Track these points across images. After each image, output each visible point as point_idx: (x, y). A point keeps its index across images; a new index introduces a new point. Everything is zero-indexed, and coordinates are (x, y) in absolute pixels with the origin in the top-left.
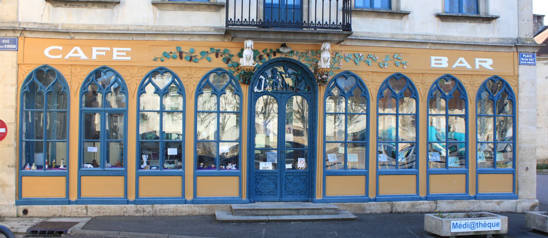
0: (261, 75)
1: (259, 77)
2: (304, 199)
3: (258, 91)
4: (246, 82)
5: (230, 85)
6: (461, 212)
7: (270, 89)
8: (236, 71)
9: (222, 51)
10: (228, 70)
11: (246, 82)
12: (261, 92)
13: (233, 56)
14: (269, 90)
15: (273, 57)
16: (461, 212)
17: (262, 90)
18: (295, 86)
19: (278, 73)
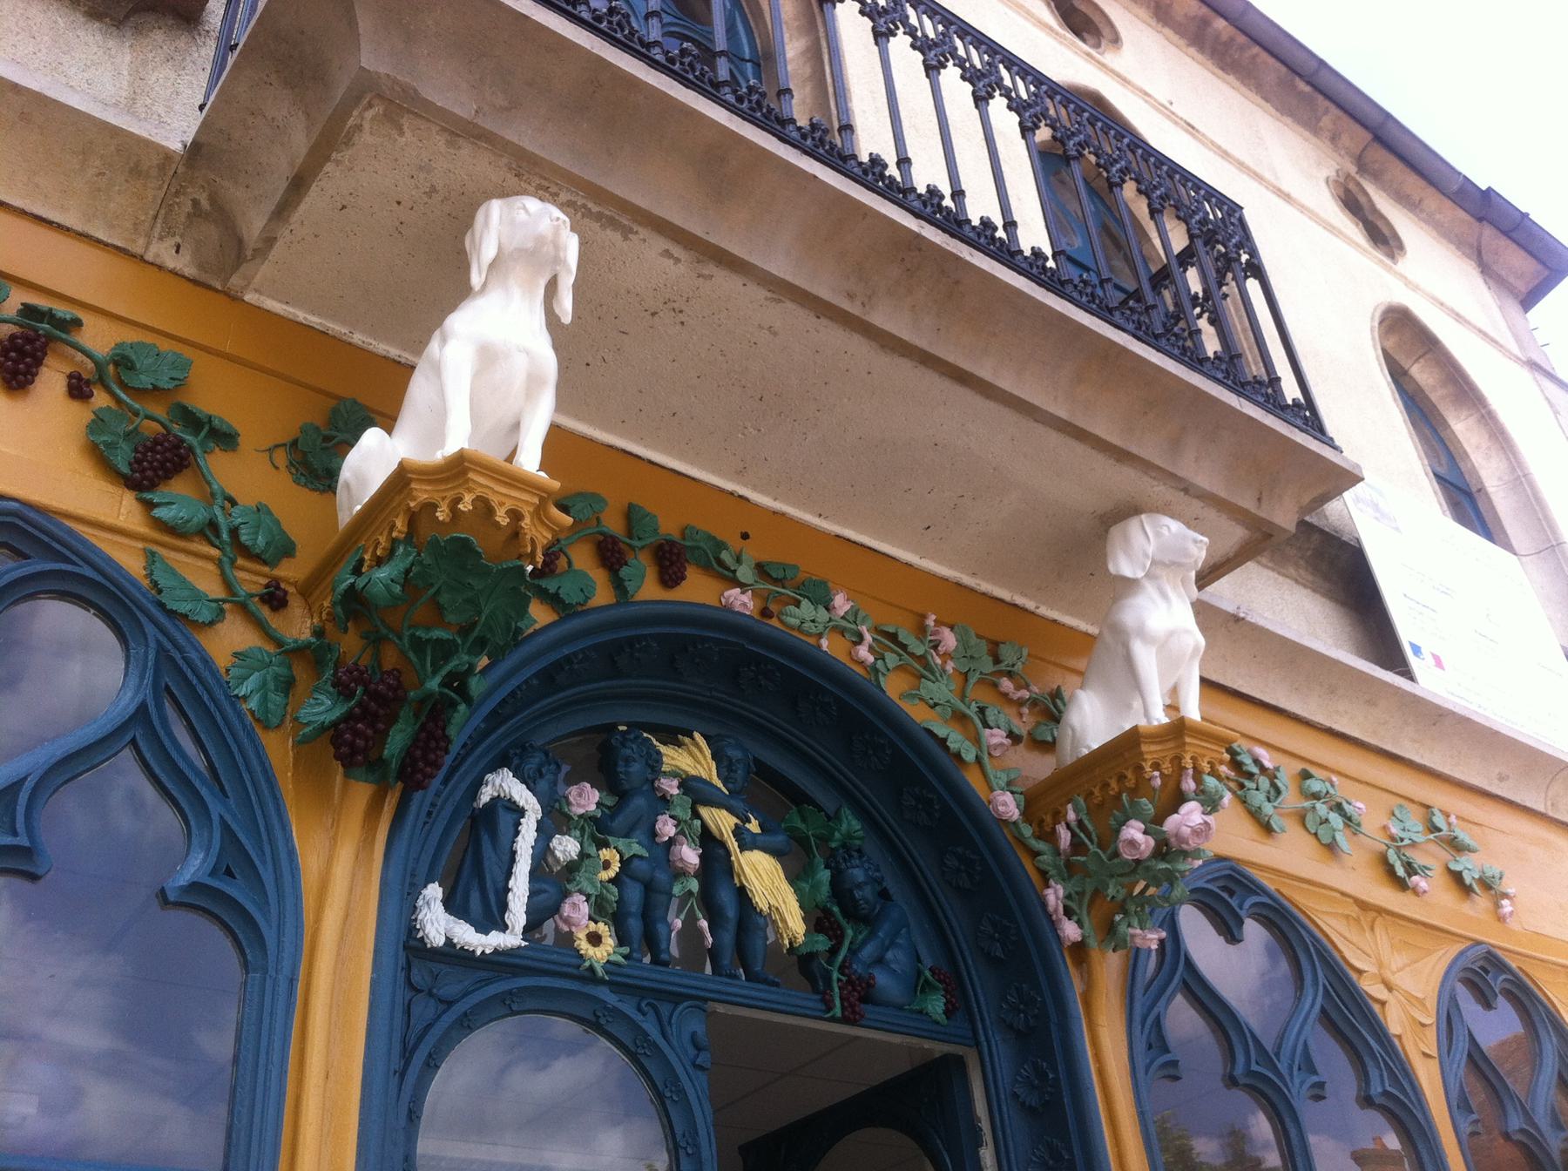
0: (494, 767)
1: (479, 783)
2: (1291, 1043)
3: (467, 936)
4: (397, 741)
5: (138, 733)
6: (1558, 422)
7: (595, 939)
8: (243, 608)
9: (98, 338)
10: (131, 562)
11: (397, 741)
12: (499, 962)
13: (226, 439)
14: (584, 946)
15: (649, 590)
16: (1558, 422)
17: (511, 939)
18: (833, 952)
19: (671, 787)
